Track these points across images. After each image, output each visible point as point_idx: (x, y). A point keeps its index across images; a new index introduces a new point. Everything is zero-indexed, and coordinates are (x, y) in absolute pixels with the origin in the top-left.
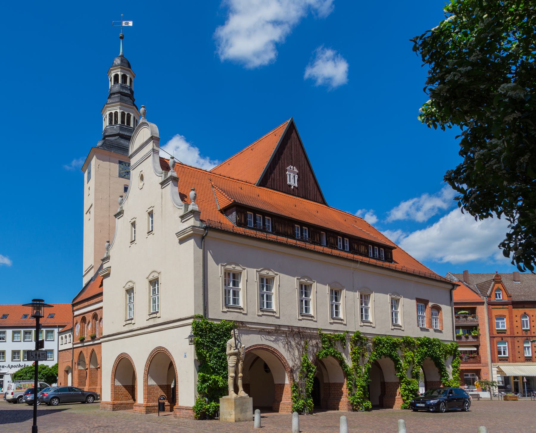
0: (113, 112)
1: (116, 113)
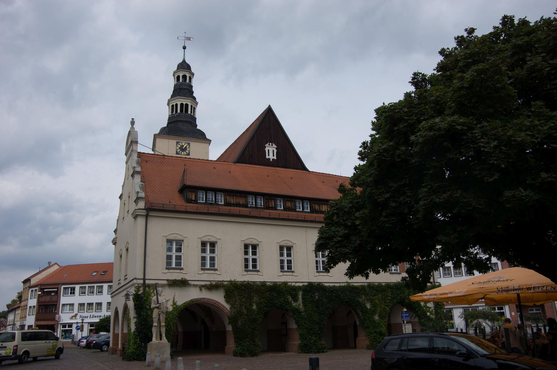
0: (174, 104)
1: (177, 105)
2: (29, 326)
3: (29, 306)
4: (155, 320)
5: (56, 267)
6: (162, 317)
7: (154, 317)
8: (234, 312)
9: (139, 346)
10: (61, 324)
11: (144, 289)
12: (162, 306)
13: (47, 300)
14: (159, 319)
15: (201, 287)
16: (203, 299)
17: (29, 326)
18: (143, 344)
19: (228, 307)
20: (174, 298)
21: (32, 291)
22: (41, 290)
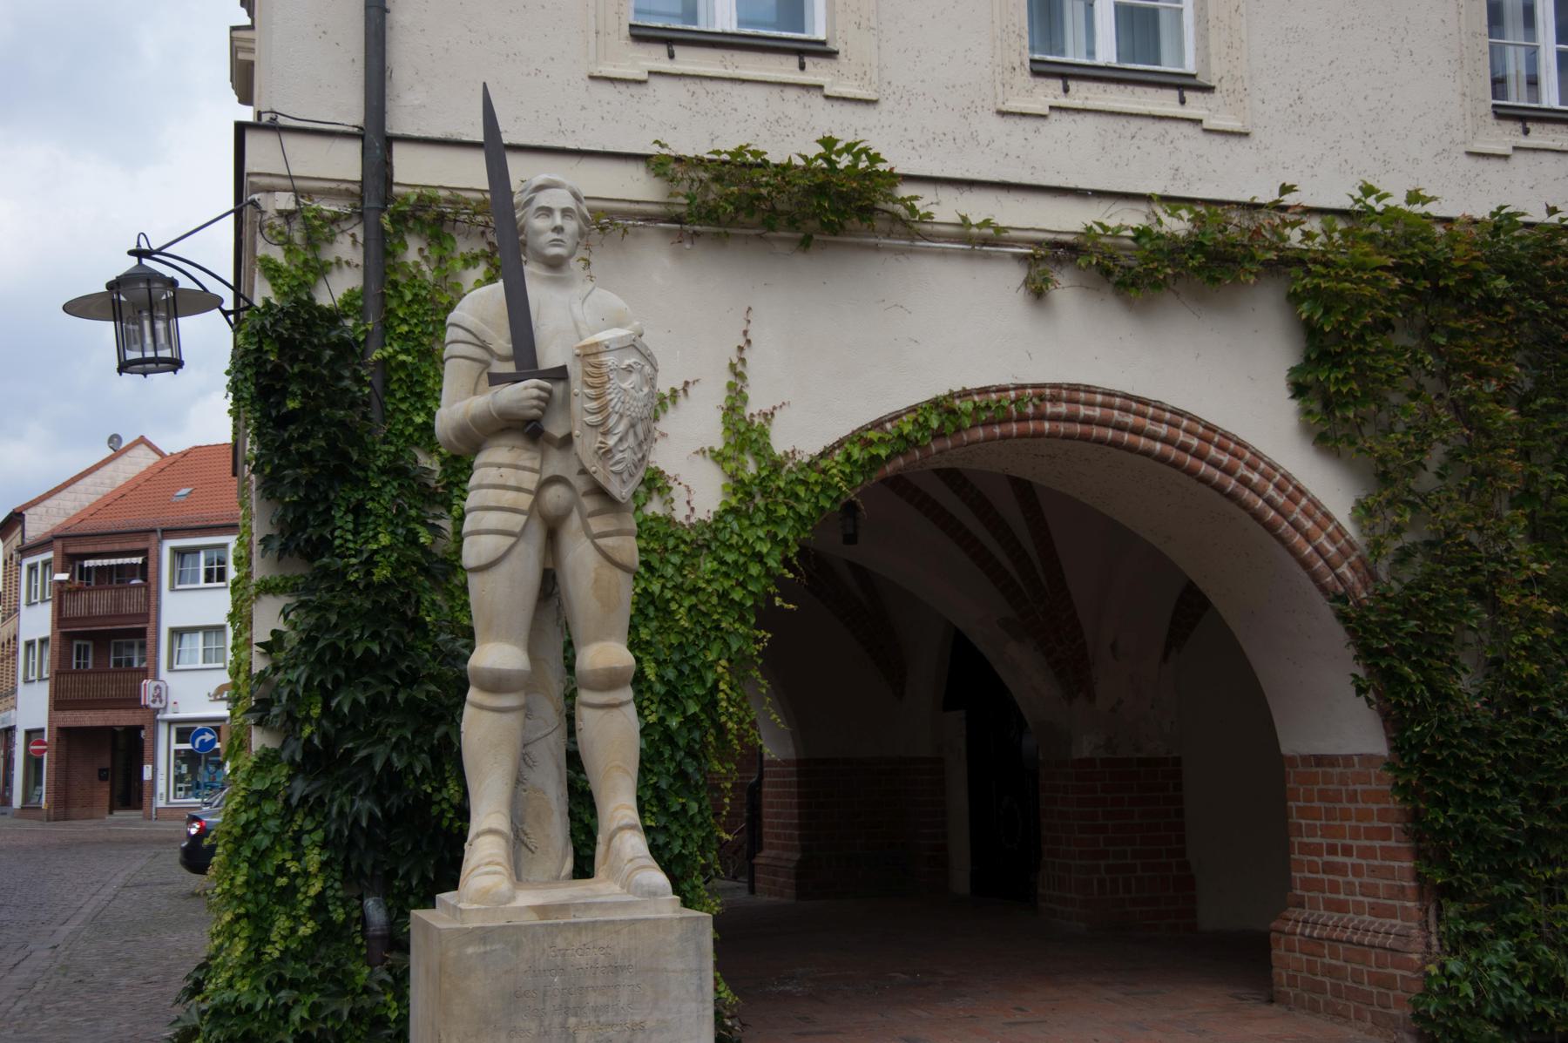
2: (29, 733)
3: (23, 638)
4: (498, 594)
5: (141, 461)
6: (596, 570)
7: (474, 551)
8: (1404, 556)
9: (329, 932)
10: (171, 722)
11: (381, 254)
12: (582, 405)
13: (97, 611)
14: (550, 586)
15: (1048, 260)
16: (1057, 392)
17: (29, 733)
18: (375, 910)
19: (1331, 490)
20: (738, 373)
21: (32, 568)
22: (71, 561)
